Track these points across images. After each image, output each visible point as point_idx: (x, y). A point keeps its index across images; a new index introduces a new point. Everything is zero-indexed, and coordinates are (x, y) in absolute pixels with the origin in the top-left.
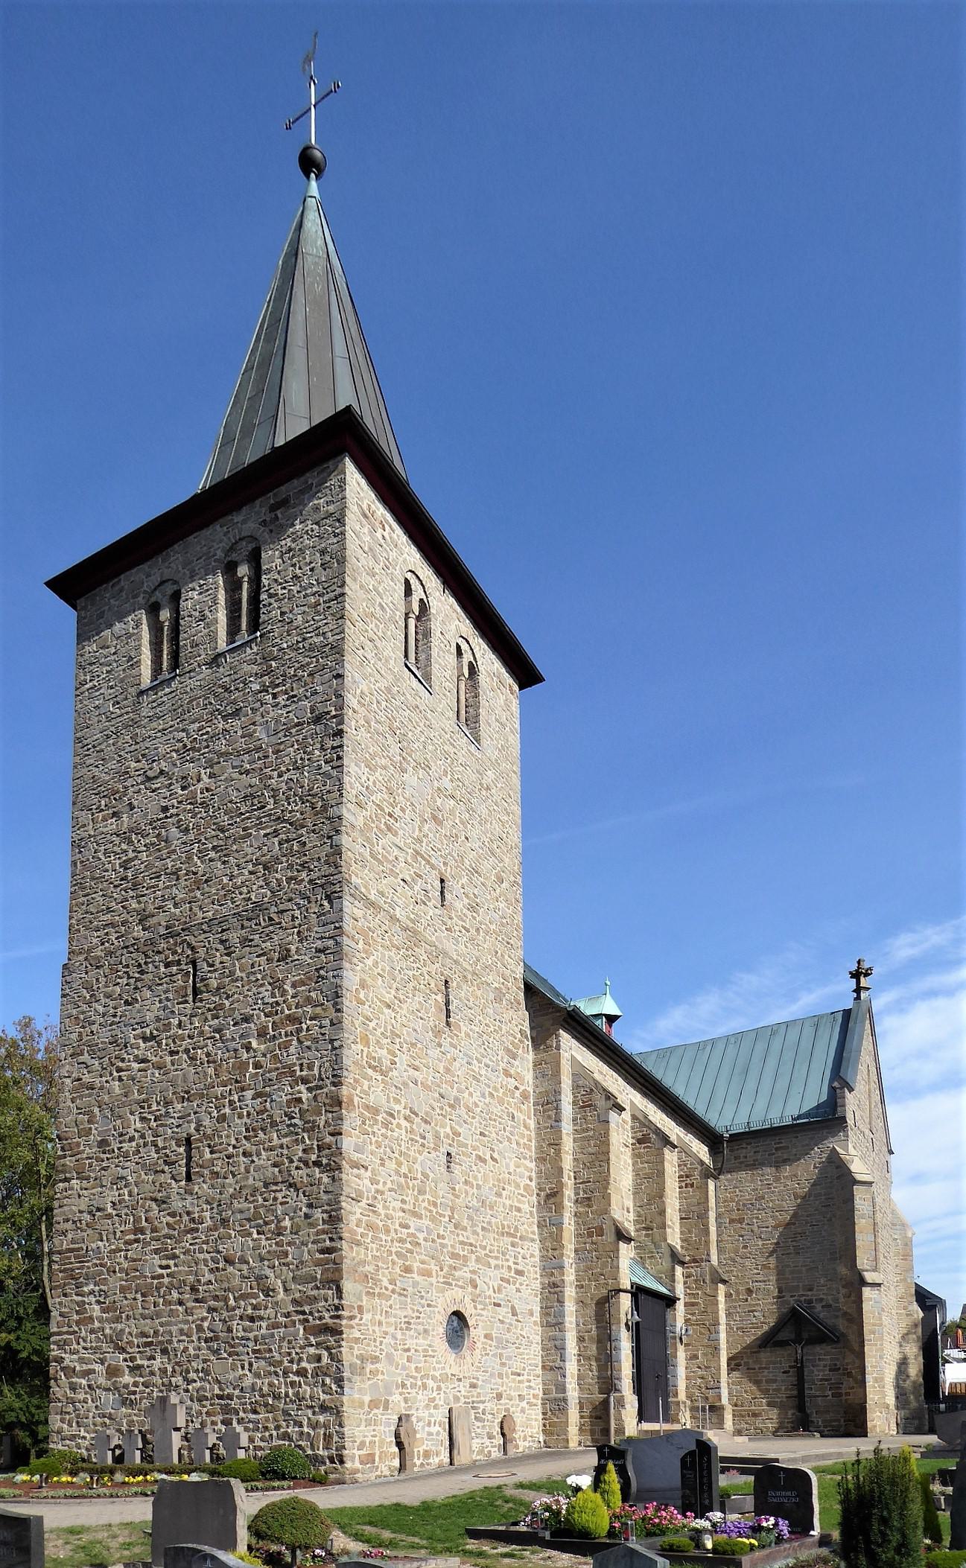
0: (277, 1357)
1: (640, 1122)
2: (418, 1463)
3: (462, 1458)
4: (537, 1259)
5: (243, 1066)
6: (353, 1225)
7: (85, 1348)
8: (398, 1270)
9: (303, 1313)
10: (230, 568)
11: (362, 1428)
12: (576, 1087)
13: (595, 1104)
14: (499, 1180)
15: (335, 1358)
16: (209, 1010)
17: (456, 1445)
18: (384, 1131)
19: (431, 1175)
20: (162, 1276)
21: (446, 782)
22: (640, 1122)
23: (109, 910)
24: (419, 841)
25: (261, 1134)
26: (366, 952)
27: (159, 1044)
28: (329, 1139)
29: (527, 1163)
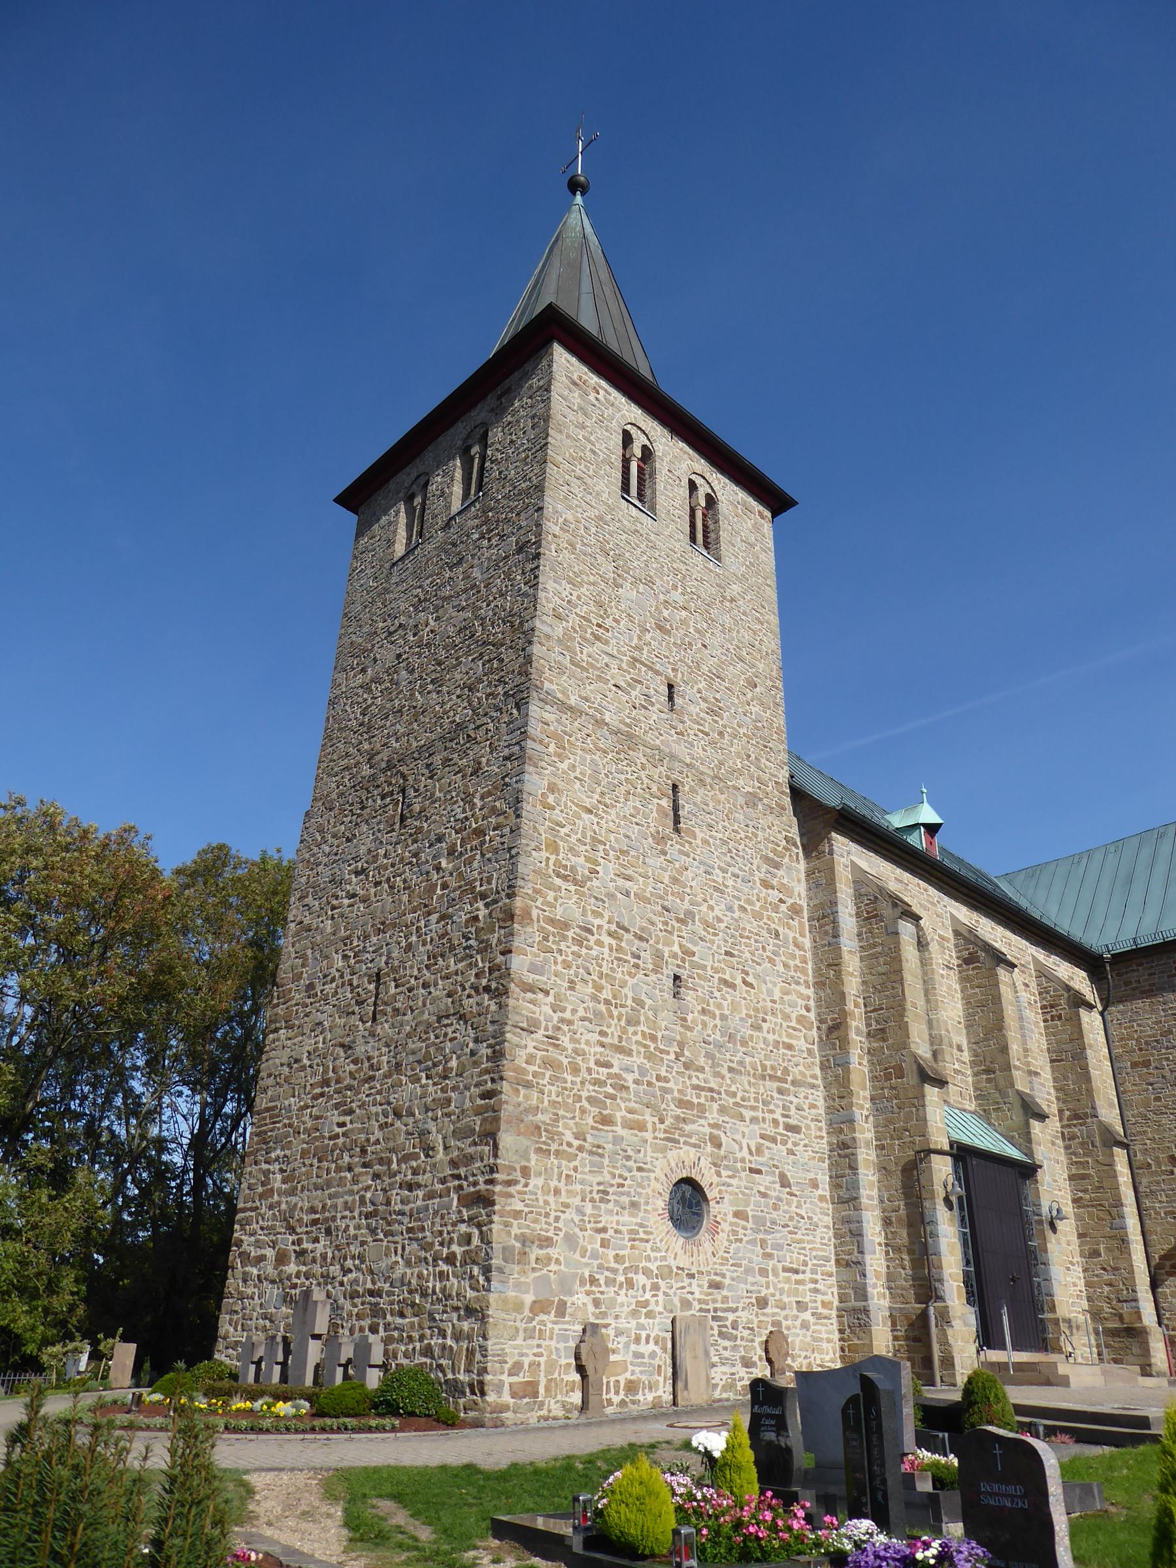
1: (965, 938)
2: (616, 1399)
3: (694, 1395)
4: (822, 1111)
5: (431, 889)
6: (520, 1062)
7: (262, 1228)
8: (590, 1121)
10: (465, 453)
11: (519, 1341)
12: (858, 896)
13: (883, 914)
14: (756, 1010)
15: (485, 1239)
16: (411, 835)
17: (682, 1376)
18: (575, 948)
19: (649, 1002)
20: (337, 1136)
21: (676, 596)
22: (965, 938)
23: (347, 755)
24: (638, 648)
25: (440, 961)
26: (559, 755)
27: (367, 876)
28: (500, 959)
29: (802, 989)
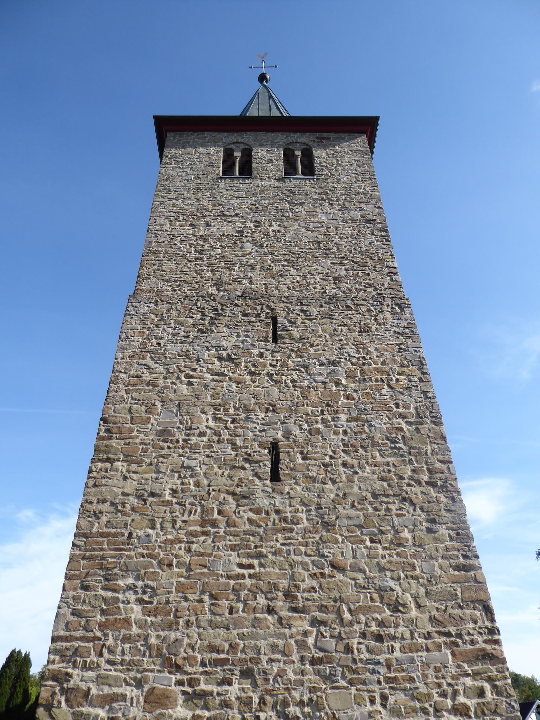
0: (423, 689)
7: (109, 662)
9: (448, 634)
25: (361, 451)
